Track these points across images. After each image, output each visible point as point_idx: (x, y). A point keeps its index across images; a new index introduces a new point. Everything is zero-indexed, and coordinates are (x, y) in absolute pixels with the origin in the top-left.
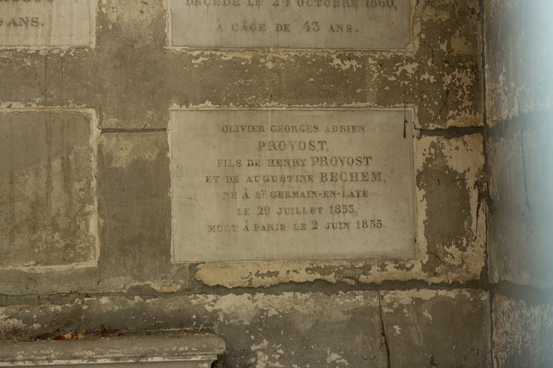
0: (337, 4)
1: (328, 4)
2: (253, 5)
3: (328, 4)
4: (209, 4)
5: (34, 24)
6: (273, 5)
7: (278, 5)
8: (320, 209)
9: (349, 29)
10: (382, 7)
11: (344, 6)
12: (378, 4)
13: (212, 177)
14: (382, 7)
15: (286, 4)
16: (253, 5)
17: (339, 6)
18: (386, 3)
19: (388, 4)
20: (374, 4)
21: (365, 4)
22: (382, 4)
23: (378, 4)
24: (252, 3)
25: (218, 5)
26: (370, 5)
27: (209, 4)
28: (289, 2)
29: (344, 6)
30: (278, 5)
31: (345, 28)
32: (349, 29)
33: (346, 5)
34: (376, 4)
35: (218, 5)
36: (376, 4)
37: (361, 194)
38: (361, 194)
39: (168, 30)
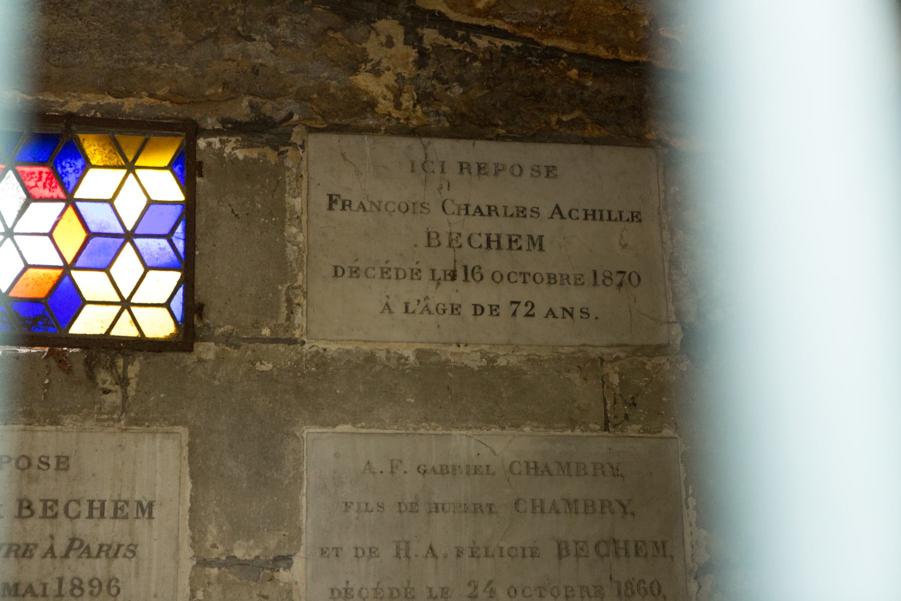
0: (570, 594)
1: (556, 594)
2: (436, 598)
3: (556, 594)
4: (367, 597)
5: (533, 214)
6: (469, 597)
7: (476, 597)
8: (338, 551)
9: (585, 313)
10: (643, 597)
11: (583, 597)
12: (636, 591)
13: (331, 549)
14: (643, 597)
15: (488, 594)
16: (436, 598)
17: (573, 596)
18: (649, 590)
19: (652, 591)
20: (629, 592)
21: (616, 593)
22: (642, 591)
23: (636, 591)
24: (434, 594)
25: (381, 598)
26: (623, 592)
27: (367, 597)
28: (494, 592)
29: (583, 597)
30: (476, 597)
31: (577, 314)
32: (585, 313)
33: (586, 594)
34: (633, 593)
35: (381, 598)
36: (633, 593)
37: (528, 553)
38: (528, 553)
39: (363, 427)
